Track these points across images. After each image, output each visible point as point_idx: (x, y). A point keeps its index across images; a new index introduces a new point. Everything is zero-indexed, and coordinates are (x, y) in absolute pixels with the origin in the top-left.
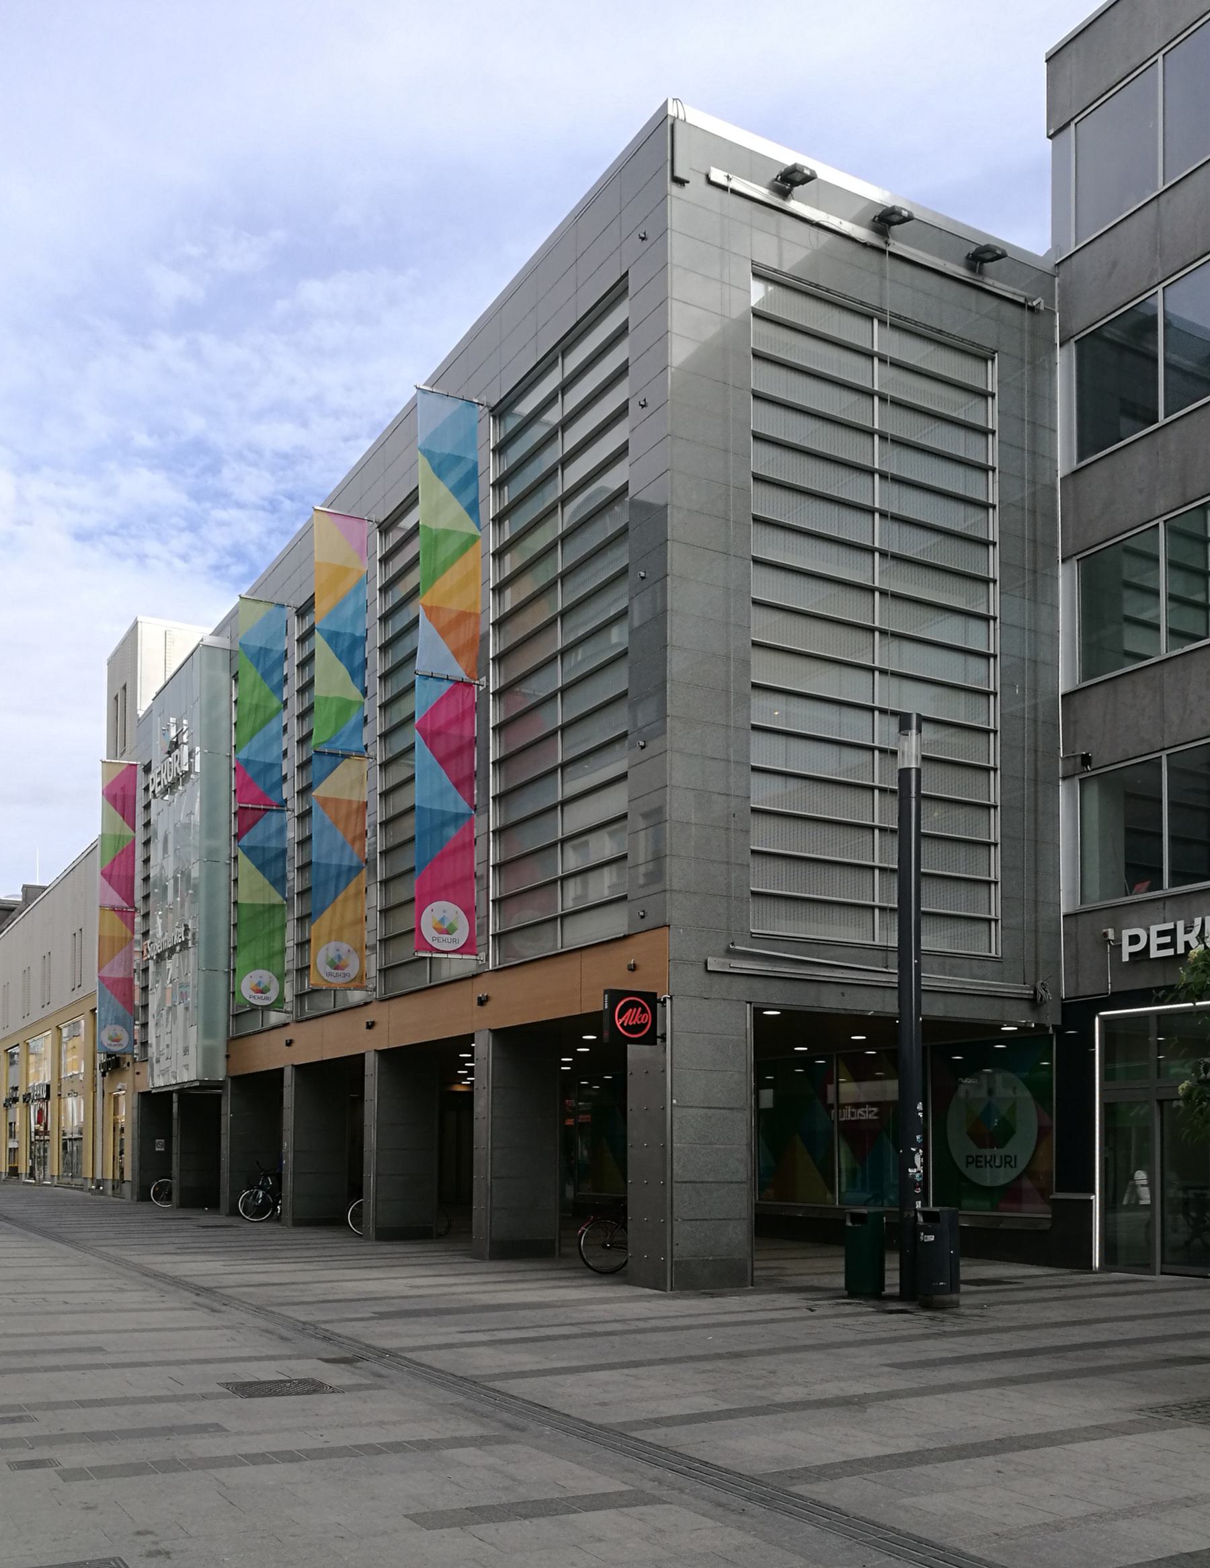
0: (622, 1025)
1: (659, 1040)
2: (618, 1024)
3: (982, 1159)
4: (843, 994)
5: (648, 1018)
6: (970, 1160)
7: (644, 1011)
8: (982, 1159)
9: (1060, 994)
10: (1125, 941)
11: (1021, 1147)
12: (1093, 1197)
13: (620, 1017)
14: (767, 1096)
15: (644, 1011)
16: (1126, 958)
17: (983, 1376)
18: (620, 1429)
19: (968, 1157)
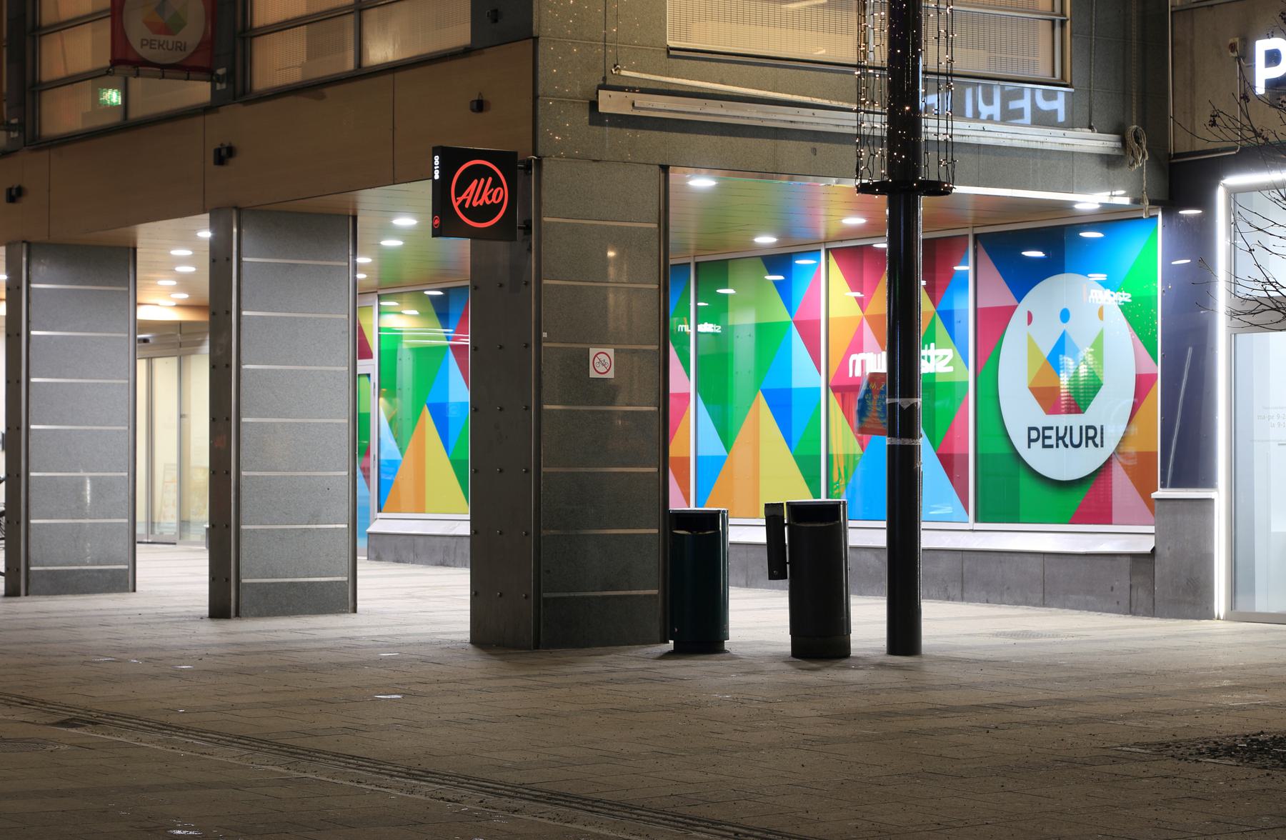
0: (461, 206)
1: (519, 233)
2: (456, 205)
3: (1052, 433)
4: (814, 151)
5: (503, 193)
6: (1034, 435)
7: (496, 183)
8: (1052, 433)
9: (1166, 146)
10: (1260, 58)
11: (1111, 412)
12: (915, 400)
13: (458, 194)
14: (437, 222)
15: (496, 183)
16: (1260, 89)
17: (1033, 712)
18: (855, 417)
19: (1030, 429)
